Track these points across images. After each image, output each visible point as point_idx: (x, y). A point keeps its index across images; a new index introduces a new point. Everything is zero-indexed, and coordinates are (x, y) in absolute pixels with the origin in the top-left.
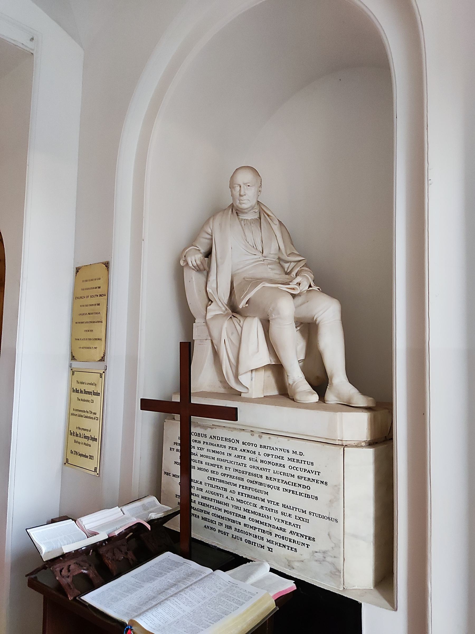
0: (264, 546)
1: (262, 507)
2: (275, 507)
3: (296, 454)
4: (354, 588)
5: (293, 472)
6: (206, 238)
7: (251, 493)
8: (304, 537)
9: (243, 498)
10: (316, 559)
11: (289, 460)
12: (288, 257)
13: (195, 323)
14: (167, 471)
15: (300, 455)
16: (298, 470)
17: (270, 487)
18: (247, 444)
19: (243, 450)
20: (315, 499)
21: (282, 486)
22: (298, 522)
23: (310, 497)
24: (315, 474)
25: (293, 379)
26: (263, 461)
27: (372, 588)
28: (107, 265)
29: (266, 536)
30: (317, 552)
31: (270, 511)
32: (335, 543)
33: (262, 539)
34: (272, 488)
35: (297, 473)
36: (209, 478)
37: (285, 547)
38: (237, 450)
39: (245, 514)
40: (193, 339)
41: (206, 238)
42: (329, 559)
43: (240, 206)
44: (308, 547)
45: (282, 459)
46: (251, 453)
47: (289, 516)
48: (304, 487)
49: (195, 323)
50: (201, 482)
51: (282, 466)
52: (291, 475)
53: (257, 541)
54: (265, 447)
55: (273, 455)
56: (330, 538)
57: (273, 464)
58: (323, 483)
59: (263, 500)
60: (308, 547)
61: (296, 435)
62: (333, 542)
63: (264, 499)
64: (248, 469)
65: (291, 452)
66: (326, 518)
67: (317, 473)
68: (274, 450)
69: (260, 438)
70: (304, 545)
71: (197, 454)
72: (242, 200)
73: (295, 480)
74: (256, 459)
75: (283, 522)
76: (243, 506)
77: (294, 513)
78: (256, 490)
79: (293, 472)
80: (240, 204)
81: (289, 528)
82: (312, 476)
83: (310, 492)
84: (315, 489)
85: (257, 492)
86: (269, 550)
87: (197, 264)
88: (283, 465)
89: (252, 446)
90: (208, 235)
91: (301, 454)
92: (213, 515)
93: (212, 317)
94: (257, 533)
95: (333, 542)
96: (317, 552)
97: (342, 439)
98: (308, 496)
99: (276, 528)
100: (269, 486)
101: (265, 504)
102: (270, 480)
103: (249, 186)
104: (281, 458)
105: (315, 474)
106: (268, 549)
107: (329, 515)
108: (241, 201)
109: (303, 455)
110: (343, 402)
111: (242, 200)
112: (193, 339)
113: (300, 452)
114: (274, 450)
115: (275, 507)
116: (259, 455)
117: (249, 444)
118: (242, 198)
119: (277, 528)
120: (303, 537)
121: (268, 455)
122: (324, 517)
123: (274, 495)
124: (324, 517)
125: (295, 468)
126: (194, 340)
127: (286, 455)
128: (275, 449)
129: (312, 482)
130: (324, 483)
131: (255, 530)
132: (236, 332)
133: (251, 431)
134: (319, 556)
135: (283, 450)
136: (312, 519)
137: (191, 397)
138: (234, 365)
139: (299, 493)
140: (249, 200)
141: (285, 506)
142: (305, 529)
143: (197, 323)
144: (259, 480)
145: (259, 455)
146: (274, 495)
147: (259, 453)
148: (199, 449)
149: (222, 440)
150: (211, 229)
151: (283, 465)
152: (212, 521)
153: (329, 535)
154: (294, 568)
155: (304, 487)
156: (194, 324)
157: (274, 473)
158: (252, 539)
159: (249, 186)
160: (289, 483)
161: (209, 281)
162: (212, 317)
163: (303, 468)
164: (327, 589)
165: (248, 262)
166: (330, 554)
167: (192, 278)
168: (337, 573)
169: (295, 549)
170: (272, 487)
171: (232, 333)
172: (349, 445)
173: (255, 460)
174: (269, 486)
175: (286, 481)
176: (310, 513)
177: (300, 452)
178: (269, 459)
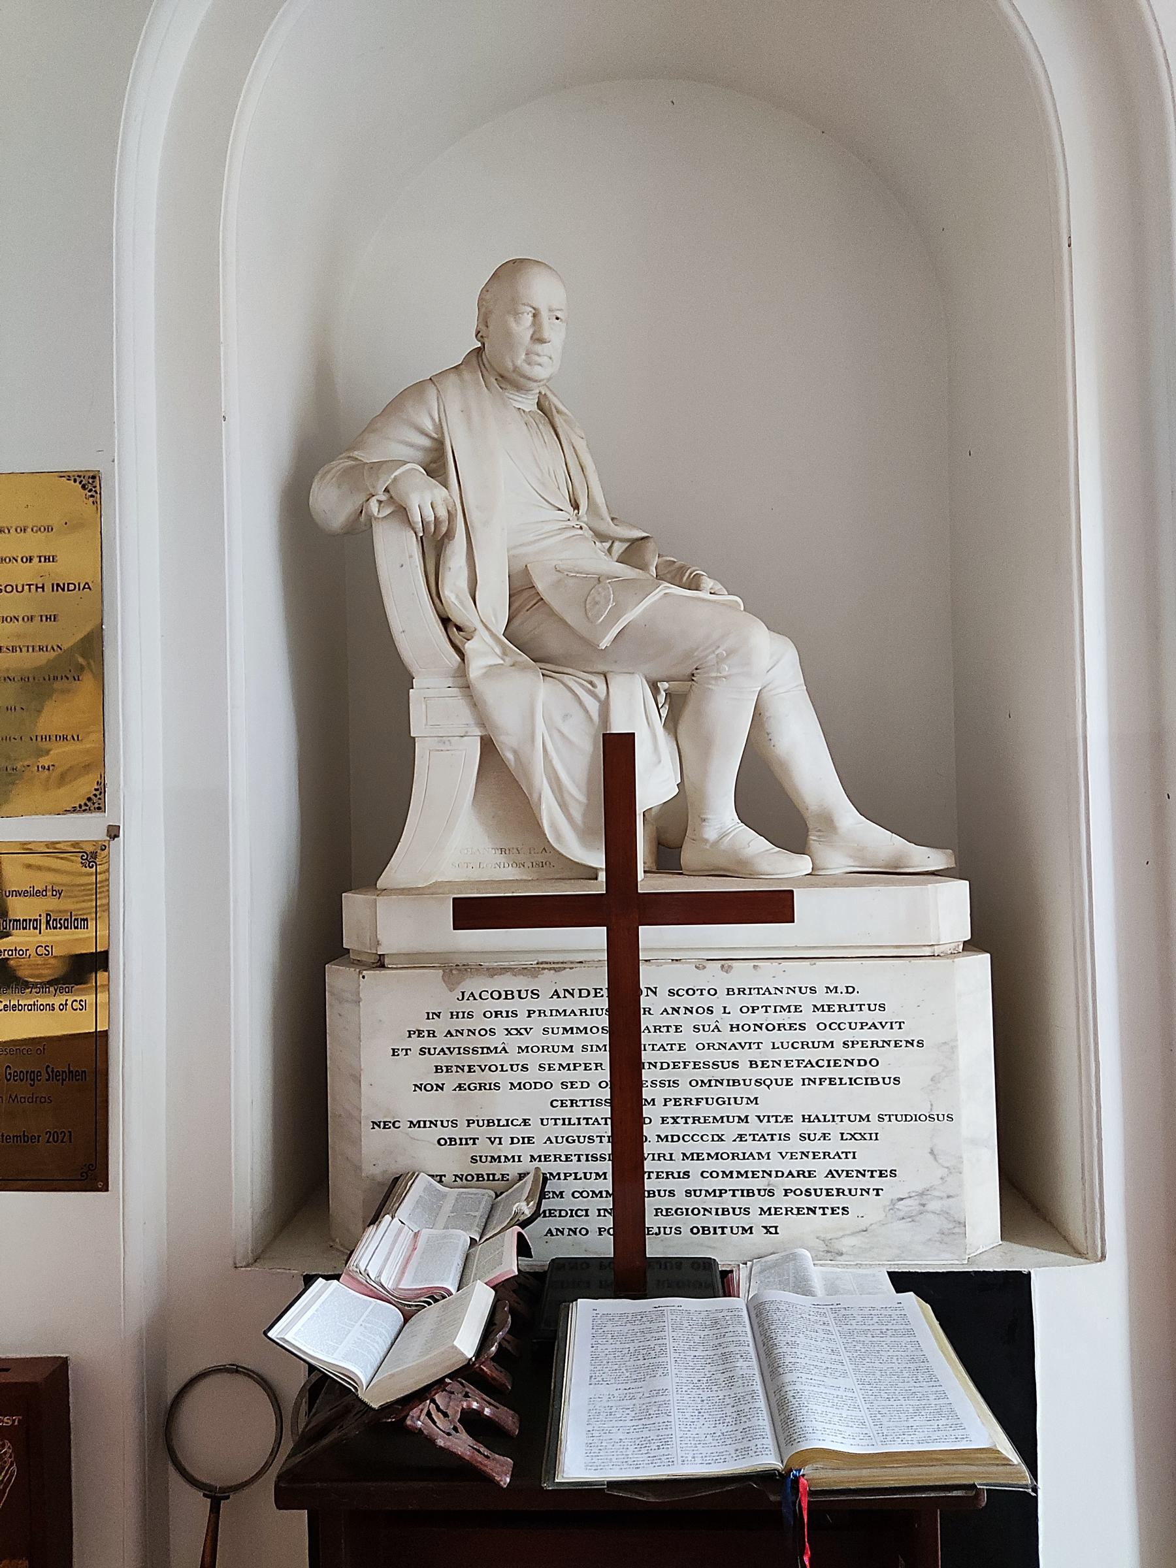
0: (751, 1228)
1: (741, 1136)
2: (783, 1128)
3: (836, 992)
4: (978, 1252)
5: (828, 1036)
6: (412, 446)
7: (703, 1110)
8: (868, 1174)
9: (680, 1129)
10: (901, 1214)
11: (816, 1010)
12: (616, 527)
13: (413, 688)
14: (385, 1117)
15: (847, 992)
16: (842, 1028)
17: (763, 1085)
18: (684, 992)
19: (673, 1009)
20: (892, 1083)
21: (797, 1074)
22: (850, 1146)
23: (879, 1083)
24: (892, 1028)
25: (719, 826)
26: (738, 1025)
27: (1001, 1242)
28: (90, 483)
29: (755, 1203)
30: (902, 1199)
31: (765, 1140)
32: (947, 1168)
33: (747, 1211)
34: (768, 1086)
35: (838, 1037)
36: (555, 1104)
37: (814, 1212)
38: (651, 1012)
39: (688, 1165)
40: (412, 735)
41: (412, 446)
42: (934, 1205)
43: (526, 368)
44: (878, 1194)
45: (829, 1011)
46: (697, 1012)
47: (822, 1139)
48: (863, 1063)
49: (413, 688)
50: (524, 1120)
51: (797, 1027)
52: (825, 1042)
53: (730, 1220)
54: (741, 991)
55: (770, 1006)
56: (935, 1159)
57: (770, 1027)
58: (912, 1044)
59: (744, 1120)
60: (878, 1194)
61: (835, 951)
62: (943, 1167)
63: (746, 1117)
64: (691, 1054)
65: (821, 990)
66: (923, 1118)
67: (896, 1026)
68: (770, 994)
69: (727, 972)
70: (868, 1193)
71: (504, 1049)
72: (538, 355)
73: (839, 1052)
74: (504, 1048)
75: (807, 1157)
76: (678, 1148)
77: (834, 1129)
78: (720, 1100)
79: (828, 1036)
80: (529, 364)
81: (821, 1166)
82: (880, 1035)
83: (876, 1072)
84: (890, 1061)
85: (724, 1103)
86: (768, 1232)
87: (435, 517)
88: (800, 1025)
89: (702, 994)
90: (423, 437)
91: (850, 990)
92: (577, 1195)
93: (484, 670)
94: (728, 1201)
95: (943, 1167)
96: (902, 1199)
97: (939, 940)
98: (874, 1081)
99: (785, 1175)
100: (758, 1082)
101: (753, 1127)
102: (763, 1067)
103: (557, 319)
104: (826, 1008)
105: (892, 1028)
106: (765, 1231)
107: (931, 1109)
108: (536, 358)
109: (856, 991)
110: (890, 868)
111: (538, 355)
112: (412, 735)
113: (847, 987)
114: (770, 994)
115: (783, 1128)
116: (725, 1012)
117: (691, 992)
118: (539, 348)
119: (790, 1173)
120: (864, 1176)
121: (753, 1010)
122: (917, 1118)
123: (773, 1100)
124: (917, 1118)
125: (834, 1026)
126: (414, 738)
127: (806, 1001)
128: (773, 991)
129: (883, 1047)
130: (915, 1043)
131: (720, 1196)
132: (581, 713)
133: (673, 960)
134: (911, 1205)
135: (797, 990)
136: (887, 1129)
137: (604, 880)
138: (580, 803)
139: (848, 1080)
140: (550, 358)
141: (809, 1119)
142: (868, 1156)
143: (417, 689)
144: (731, 1074)
145: (725, 1012)
146: (773, 1100)
147: (725, 1008)
148: (514, 1032)
149: (596, 996)
150: (433, 419)
151: (800, 1025)
152: (574, 1213)
153: (932, 1152)
154: (842, 1254)
155: (863, 1063)
156: (411, 690)
157: (774, 1048)
158: (712, 1221)
159: (557, 319)
160: (820, 1063)
161: (450, 569)
162: (486, 673)
163: (858, 1021)
164: (945, 1271)
165: (548, 527)
166: (936, 1193)
167: (411, 557)
168: (957, 1230)
169: (843, 1209)
170: (768, 1082)
171: (566, 717)
172: (942, 955)
173: (711, 1030)
174: (758, 1082)
175: (810, 1061)
176: (880, 1118)
177: (847, 987)
178: (760, 1017)
